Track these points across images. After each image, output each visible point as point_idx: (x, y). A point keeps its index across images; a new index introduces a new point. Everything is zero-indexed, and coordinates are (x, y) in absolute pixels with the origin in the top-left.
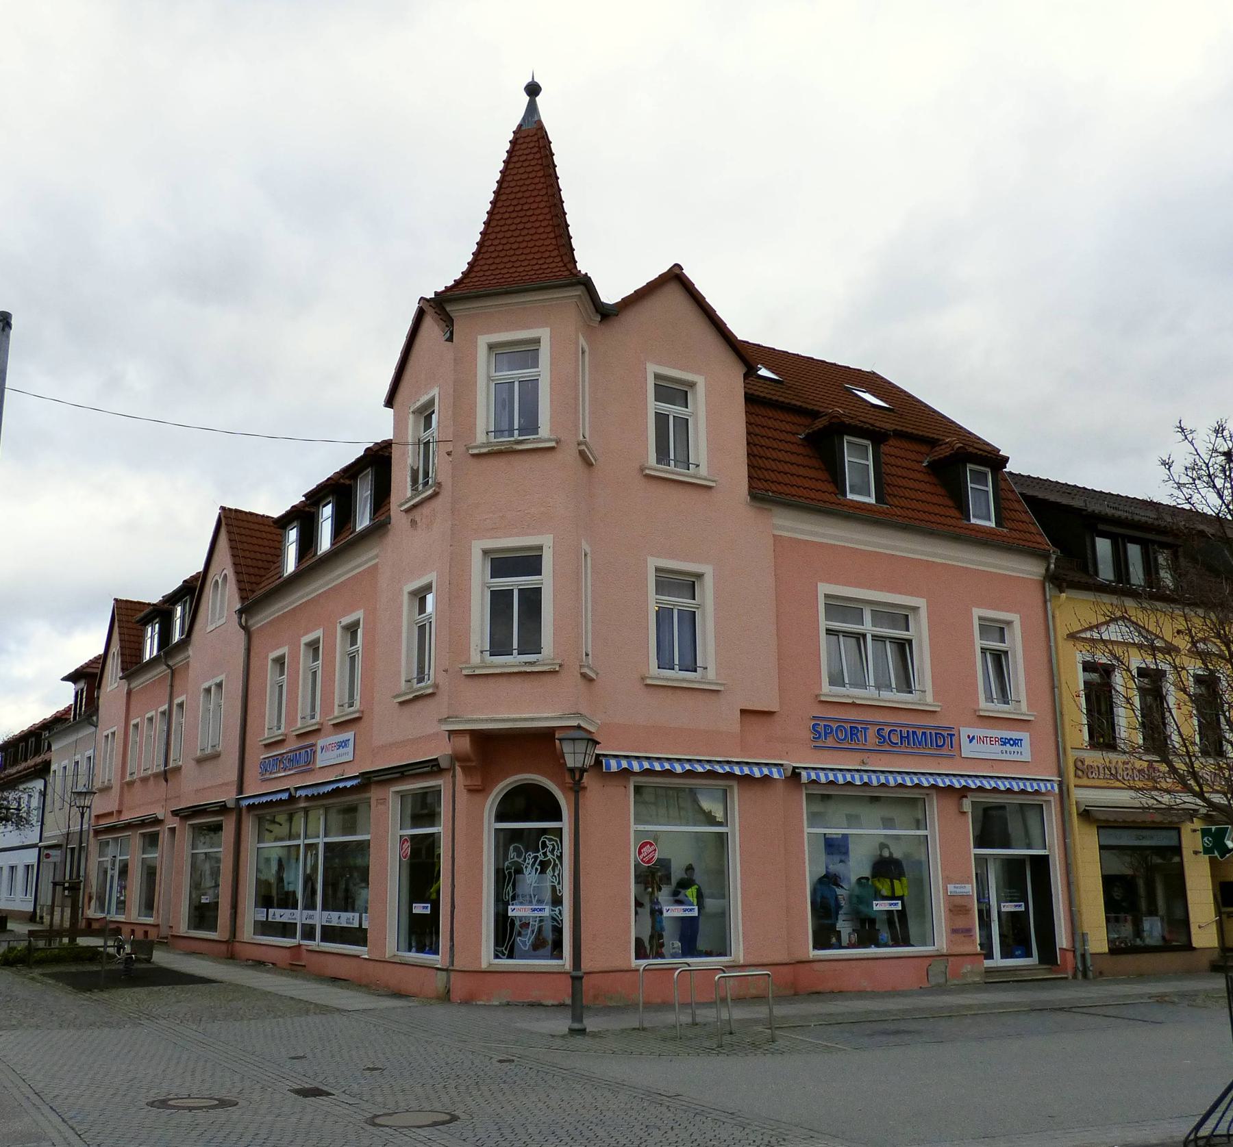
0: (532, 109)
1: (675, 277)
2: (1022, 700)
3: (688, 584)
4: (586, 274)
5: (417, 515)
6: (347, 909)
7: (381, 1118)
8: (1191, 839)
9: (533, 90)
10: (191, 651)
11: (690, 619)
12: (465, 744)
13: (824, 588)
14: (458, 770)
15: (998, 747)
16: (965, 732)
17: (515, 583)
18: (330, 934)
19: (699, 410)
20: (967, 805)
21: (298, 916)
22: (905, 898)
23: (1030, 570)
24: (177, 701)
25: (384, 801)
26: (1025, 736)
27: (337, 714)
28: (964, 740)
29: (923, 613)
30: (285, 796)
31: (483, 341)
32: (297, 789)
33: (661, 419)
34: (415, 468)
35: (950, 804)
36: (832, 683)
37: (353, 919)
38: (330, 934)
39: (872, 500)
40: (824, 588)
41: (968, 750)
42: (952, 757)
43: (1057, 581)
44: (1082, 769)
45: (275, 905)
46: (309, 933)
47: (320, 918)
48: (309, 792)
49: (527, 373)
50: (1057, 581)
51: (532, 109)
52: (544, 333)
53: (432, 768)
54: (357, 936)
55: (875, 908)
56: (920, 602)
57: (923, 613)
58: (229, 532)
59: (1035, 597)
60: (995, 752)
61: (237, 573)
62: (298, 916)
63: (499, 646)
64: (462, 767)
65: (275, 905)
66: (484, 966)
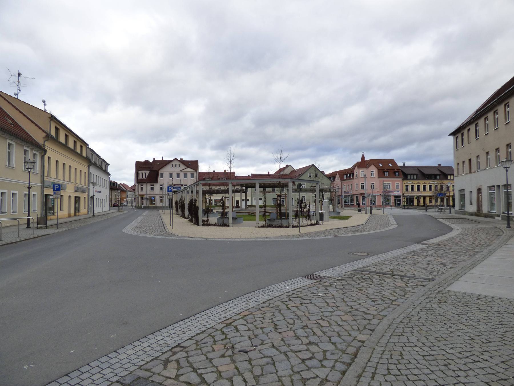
2: (399, 189)
4: (154, 159)
8: (415, 198)
11: (373, 186)
19: (374, 173)
21: (348, 203)
23: (401, 179)
43: (403, 180)
46: (349, 204)
47: (350, 203)
50: (403, 180)
53: (358, 195)
62: (348, 203)
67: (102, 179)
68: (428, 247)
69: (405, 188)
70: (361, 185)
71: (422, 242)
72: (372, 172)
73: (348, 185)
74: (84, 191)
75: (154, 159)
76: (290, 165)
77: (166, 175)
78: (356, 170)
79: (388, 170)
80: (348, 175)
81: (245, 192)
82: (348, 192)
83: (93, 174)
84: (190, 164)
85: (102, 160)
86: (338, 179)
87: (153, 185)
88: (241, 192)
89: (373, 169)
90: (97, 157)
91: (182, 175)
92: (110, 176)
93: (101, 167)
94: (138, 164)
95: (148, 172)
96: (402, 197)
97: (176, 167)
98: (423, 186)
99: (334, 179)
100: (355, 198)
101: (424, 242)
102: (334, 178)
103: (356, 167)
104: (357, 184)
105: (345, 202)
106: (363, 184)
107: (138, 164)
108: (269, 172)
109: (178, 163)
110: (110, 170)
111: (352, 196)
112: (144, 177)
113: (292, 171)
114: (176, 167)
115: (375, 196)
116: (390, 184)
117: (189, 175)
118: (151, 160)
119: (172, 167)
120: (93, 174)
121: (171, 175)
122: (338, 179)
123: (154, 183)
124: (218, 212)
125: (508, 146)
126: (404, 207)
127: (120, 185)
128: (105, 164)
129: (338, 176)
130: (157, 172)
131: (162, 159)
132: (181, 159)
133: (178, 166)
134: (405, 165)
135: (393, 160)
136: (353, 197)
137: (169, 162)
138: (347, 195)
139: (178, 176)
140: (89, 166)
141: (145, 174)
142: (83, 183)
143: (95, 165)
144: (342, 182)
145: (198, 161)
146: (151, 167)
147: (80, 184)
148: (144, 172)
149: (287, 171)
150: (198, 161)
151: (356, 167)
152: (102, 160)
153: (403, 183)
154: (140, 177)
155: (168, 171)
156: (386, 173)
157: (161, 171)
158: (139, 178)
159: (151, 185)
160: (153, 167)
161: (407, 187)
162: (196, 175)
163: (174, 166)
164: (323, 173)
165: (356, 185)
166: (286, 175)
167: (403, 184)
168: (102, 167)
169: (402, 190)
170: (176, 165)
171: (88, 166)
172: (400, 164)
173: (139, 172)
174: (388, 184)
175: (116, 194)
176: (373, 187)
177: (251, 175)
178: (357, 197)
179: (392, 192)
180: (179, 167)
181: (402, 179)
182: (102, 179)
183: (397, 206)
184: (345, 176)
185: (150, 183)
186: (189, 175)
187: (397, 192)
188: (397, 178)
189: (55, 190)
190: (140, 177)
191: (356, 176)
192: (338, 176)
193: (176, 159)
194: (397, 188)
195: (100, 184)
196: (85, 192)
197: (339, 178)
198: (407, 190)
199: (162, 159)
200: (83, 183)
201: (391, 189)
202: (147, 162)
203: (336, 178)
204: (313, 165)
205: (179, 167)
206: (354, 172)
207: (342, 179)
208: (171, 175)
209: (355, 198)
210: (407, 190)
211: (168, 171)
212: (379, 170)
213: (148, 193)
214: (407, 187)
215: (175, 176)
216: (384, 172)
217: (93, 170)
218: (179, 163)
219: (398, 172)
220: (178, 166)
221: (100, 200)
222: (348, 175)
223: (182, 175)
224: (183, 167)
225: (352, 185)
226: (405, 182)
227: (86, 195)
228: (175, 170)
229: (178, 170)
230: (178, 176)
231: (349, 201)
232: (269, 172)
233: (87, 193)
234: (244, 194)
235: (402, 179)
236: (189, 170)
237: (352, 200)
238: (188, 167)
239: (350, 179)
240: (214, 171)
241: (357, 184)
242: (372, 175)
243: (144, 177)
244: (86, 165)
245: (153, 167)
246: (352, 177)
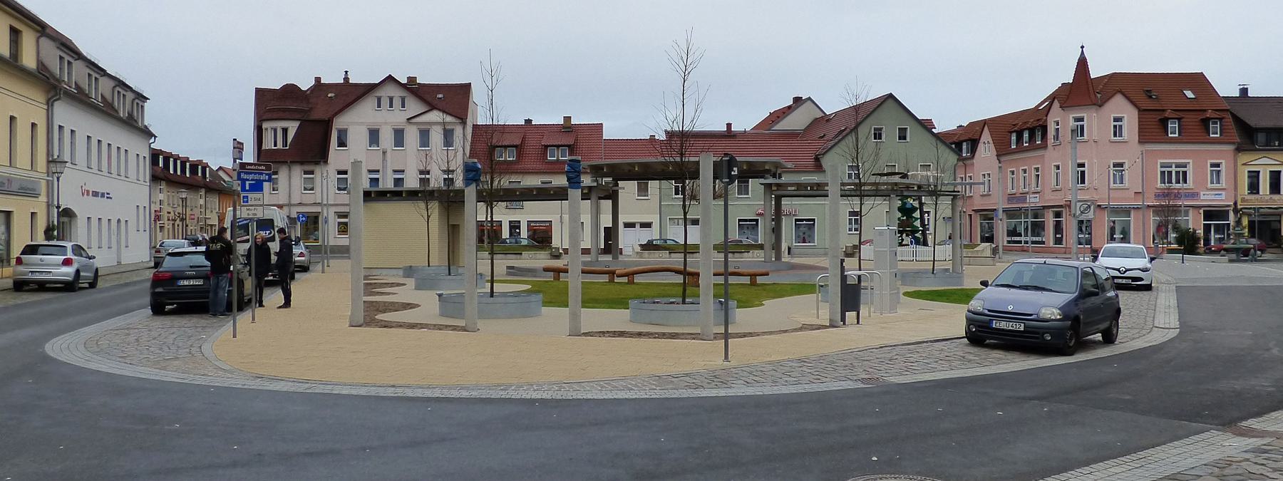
1: (390, 75)
2: (1223, 184)
4: (318, 80)
10: (974, 161)
11: (1185, 173)
13: (1159, 161)
16: (1202, 193)
18: (1033, 242)
19: (1125, 123)
20: (1202, 211)
21: (1023, 239)
24: (967, 175)
26: (1223, 193)
28: (1202, 195)
29: (1191, 164)
31: (1071, 116)
33: (1115, 126)
34: (130, 112)
35: (1196, 211)
36: (1211, 183)
37: (107, 198)
38: (1033, 242)
39: (1218, 136)
40: (1159, 161)
46: (1026, 242)
49: (1081, 123)
50: (1239, 150)
52: (1085, 115)
53: (1061, 206)
54: (1043, 243)
57: (1191, 164)
59: (1231, 155)
62: (1023, 239)
67: (105, 147)
68: (1258, 451)
69: (1244, 182)
71: (1244, 423)
72: (1116, 120)
73: (1025, 171)
74: (27, 191)
75: (318, 80)
76: (809, 99)
77: (358, 137)
78: (1056, 115)
79: (1180, 115)
80: (1026, 135)
81: (613, 196)
82: (1023, 197)
83: (72, 131)
84: (440, 96)
85: (112, 83)
86: (986, 150)
87: (312, 173)
88: (594, 196)
89: (1123, 110)
90: (88, 71)
91: (412, 136)
92: (152, 140)
93: (111, 106)
94: (262, 95)
95: (293, 127)
96: (1231, 215)
97: (391, 106)
98: (1271, 172)
99: (973, 150)
100: (1050, 220)
101: (1253, 423)
102: (974, 143)
103: (1056, 104)
104: (1058, 168)
105: (1013, 232)
107: (262, 95)
108: (729, 125)
109: (397, 93)
110: (151, 117)
111: (1037, 212)
112: (280, 146)
113: (816, 122)
114: (391, 106)
115: (1126, 211)
117: (436, 137)
118: (305, 84)
119: (379, 106)
120: (72, 131)
121: (374, 136)
122: (986, 150)
123: (317, 163)
124: (512, 268)
126: (1243, 254)
127: (221, 173)
128: (130, 96)
129: (986, 136)
130: (325, 126)
131: (346, 79)
132: (412, 80)
133: (397, 102)
135: (1200, 77)
137: (368, 89)
138: (1020, 209)
139: (399, 137)
140: (49, 104)
141: (285, 131)
142: (23, 159)
143: (80, 98)
145: (469, 85)
146: (304, 106)
148: (280, 125)
149: (796, 122)
150: (469, 85)
151: (1056, 104)
152: (112, 83)
153: (1239, 164)
154: (268, 144)
155: (362, 123)
156: (1173, 126)
157: (339, 123)
158: (263, 148)
159: (306, 173)
160: (311, 108)
161: (1254, 176)
162: (462, 138)
163: (385, 102)
164: (926, 125)
165: (1054, 170)
166: (791, 135)
167: (1240, 168)
168: (113, 108)
169: (1236, 188)
170: (391, 99)
171: (48, 104)
172: (1226, 88)
173: (265, 125)
175: (202, 202)
177: (663, 137)
178: (1058, 215)
180: (403, 106)
181: (1231, 147)
182: (105, 147)
184: (1014, 138)
185: (302, 163)
186: (436, 137)
187: (1213, 197)
188: (1215, 142)
189: (247, 188)
190: (268, 144)
192: (986, 136)
193: (390, 79)
195: (114, 170)
196: (36, 196)
197: (992, 146)
198: (1254, 187)
199: (346, 79)
200: (23, 159)
202: (290, 91)
203: (981, 147)
204: (891, 96)
205: (403, 106)
206: (1046, 120)
207: (1002, 151)
208: (374, 136)
209: (1050, 220)
210: (1254, 187)
211: (362, 123)
213: (295, 200)
214: (1254, 176)
215: (387, 138)
216: (1164, 123)
217: (65, 114)
218: (403, 93)
220: (397, 102)
221: (105, 222)
222: (1026, 135)
223: (412, 136)
224: (414, 107)
226: (1244, 158)
227: (39, 205)
228: (389, 118)
229: (397, 117)
230: (399, 137)
231: (1026, 229)
232: (729, 125)
234: (607, 205)
235: (1231, 147)
236: (435, 116)
237: (1038, 228)
238: (432, 107)
239: (1033, 147)
240: (528, 121)
241: (1058, 168)
242: (1117, 131)
243: (280, 146)
244: (40, 97)
245: (311, 108)
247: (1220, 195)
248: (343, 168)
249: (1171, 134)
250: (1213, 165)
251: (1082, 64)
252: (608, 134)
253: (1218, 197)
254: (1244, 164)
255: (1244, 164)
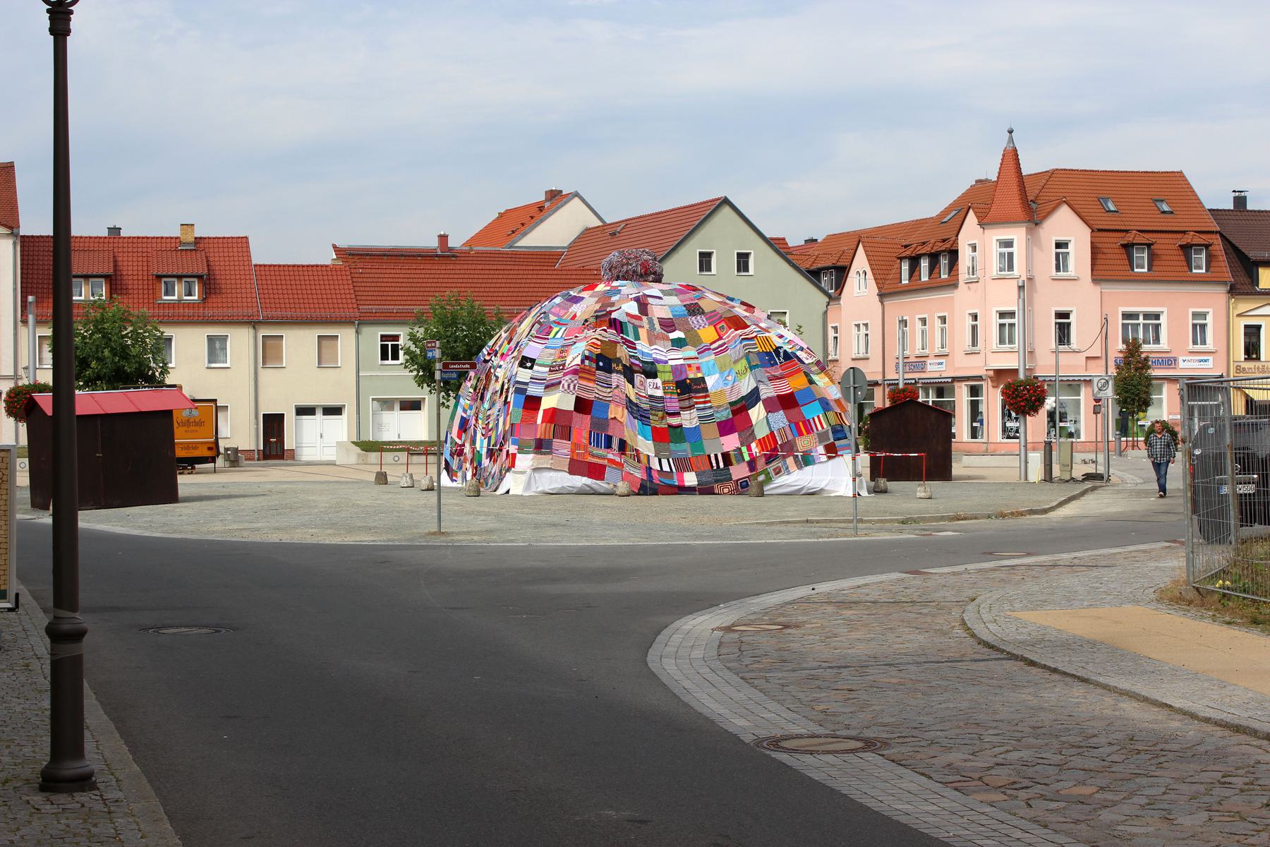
0: (1011, 140)
3: (1065, 315)
5: (971, 286)
6: (553, 413)
7: (785, 742)
9: (1011, 132)
12: (991, 373)
14: (989, 380)
15: (1197, 363)
16: (1181, 359)
17: (1007, 321)
22: (274, 473)
25: (961, 387)
26: (1210, 358)
27: (937, 350)
29: (1165, 313)
30: (913, 381)
32: (919, 379)
41: (1182, 365)
42: (1175, 368)
44: (1238, 369)
45: (1199, 342)
48: (923, 381)
50: (1234, 291)
51: (1011, 140)
53: (980, 378)
55: (19, 461)
56: (1164, 309)
58: (864, 247)
60: (1196, 365)
61: (872, 269)
63: (1002, 341)
64: (991, 381)
65: (1199, 342)
66: (999, 441)
70: (995, 321)
72: (1058, 245)
76: (577, 195)
82: (920, 363)
102: (841, 272)
104: (975, 317)
106: (1012, 314)
116: (1157, 317)
125: (1234, 191)
129: (861, 262)
134: (1249, 207)
136: (952, 393)
144: (889, 303)
147: (858, 353)
156: (1142, 256)
165: (969, 321)
174: (1147, 316)
176: (1063, 333)
178: (975, 391)
179: (1171, 362)
183: (390, 343)
184: (905, 267)
191: (973, 270)
192: (861, 262)
194: (1195, 342)
201: (1164, 344)
206: (956, 242)
209: (962, 397)
212: (1096, 231)
219: (1149, 245)
225: (943, 319)
226: (1243, 306)
233: (37, 335)
239: (935, 286)
240: (115, 231)
246: (925, 278)
247: (1206, 361)
248: (1062, 238)
249: (1137, 268)
250: (1195, 315)
251: (1011, 158)
252: (261, 255)
253: (1203, 365)
254: (1239, 315)
255: (1239, 315)
